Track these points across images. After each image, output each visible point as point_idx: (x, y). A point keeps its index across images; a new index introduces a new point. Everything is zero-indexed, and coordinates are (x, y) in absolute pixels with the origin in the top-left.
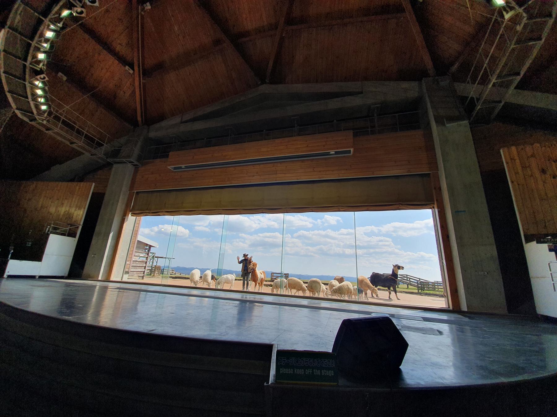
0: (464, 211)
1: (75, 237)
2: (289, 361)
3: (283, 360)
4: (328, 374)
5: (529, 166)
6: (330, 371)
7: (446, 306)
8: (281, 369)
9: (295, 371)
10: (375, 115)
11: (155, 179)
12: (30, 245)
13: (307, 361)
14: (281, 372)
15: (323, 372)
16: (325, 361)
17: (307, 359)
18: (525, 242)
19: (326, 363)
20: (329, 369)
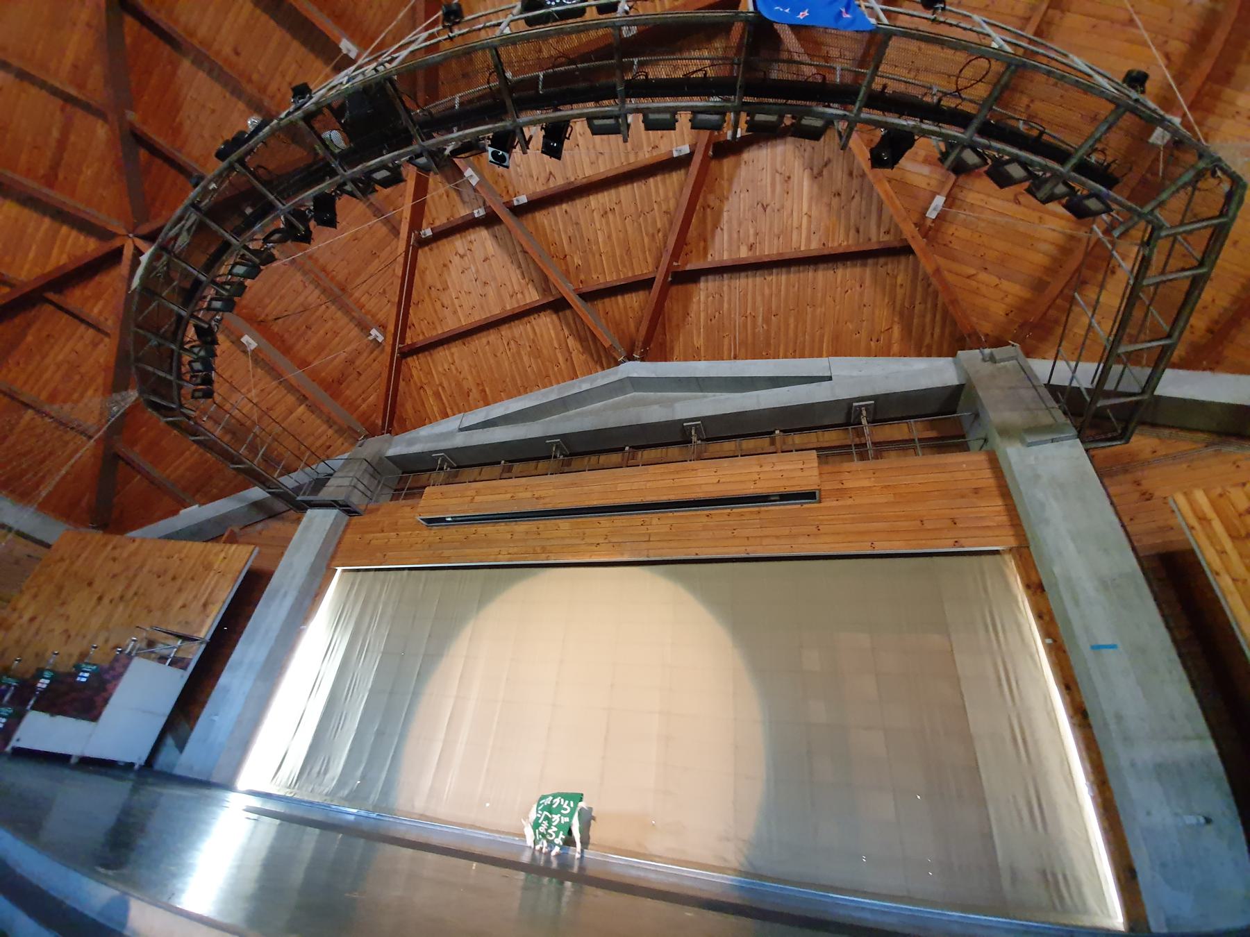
0: (1113, 647)
1: (185, 668)
7: (1094, 361)
11: (386, 543)
12: (84, 680)
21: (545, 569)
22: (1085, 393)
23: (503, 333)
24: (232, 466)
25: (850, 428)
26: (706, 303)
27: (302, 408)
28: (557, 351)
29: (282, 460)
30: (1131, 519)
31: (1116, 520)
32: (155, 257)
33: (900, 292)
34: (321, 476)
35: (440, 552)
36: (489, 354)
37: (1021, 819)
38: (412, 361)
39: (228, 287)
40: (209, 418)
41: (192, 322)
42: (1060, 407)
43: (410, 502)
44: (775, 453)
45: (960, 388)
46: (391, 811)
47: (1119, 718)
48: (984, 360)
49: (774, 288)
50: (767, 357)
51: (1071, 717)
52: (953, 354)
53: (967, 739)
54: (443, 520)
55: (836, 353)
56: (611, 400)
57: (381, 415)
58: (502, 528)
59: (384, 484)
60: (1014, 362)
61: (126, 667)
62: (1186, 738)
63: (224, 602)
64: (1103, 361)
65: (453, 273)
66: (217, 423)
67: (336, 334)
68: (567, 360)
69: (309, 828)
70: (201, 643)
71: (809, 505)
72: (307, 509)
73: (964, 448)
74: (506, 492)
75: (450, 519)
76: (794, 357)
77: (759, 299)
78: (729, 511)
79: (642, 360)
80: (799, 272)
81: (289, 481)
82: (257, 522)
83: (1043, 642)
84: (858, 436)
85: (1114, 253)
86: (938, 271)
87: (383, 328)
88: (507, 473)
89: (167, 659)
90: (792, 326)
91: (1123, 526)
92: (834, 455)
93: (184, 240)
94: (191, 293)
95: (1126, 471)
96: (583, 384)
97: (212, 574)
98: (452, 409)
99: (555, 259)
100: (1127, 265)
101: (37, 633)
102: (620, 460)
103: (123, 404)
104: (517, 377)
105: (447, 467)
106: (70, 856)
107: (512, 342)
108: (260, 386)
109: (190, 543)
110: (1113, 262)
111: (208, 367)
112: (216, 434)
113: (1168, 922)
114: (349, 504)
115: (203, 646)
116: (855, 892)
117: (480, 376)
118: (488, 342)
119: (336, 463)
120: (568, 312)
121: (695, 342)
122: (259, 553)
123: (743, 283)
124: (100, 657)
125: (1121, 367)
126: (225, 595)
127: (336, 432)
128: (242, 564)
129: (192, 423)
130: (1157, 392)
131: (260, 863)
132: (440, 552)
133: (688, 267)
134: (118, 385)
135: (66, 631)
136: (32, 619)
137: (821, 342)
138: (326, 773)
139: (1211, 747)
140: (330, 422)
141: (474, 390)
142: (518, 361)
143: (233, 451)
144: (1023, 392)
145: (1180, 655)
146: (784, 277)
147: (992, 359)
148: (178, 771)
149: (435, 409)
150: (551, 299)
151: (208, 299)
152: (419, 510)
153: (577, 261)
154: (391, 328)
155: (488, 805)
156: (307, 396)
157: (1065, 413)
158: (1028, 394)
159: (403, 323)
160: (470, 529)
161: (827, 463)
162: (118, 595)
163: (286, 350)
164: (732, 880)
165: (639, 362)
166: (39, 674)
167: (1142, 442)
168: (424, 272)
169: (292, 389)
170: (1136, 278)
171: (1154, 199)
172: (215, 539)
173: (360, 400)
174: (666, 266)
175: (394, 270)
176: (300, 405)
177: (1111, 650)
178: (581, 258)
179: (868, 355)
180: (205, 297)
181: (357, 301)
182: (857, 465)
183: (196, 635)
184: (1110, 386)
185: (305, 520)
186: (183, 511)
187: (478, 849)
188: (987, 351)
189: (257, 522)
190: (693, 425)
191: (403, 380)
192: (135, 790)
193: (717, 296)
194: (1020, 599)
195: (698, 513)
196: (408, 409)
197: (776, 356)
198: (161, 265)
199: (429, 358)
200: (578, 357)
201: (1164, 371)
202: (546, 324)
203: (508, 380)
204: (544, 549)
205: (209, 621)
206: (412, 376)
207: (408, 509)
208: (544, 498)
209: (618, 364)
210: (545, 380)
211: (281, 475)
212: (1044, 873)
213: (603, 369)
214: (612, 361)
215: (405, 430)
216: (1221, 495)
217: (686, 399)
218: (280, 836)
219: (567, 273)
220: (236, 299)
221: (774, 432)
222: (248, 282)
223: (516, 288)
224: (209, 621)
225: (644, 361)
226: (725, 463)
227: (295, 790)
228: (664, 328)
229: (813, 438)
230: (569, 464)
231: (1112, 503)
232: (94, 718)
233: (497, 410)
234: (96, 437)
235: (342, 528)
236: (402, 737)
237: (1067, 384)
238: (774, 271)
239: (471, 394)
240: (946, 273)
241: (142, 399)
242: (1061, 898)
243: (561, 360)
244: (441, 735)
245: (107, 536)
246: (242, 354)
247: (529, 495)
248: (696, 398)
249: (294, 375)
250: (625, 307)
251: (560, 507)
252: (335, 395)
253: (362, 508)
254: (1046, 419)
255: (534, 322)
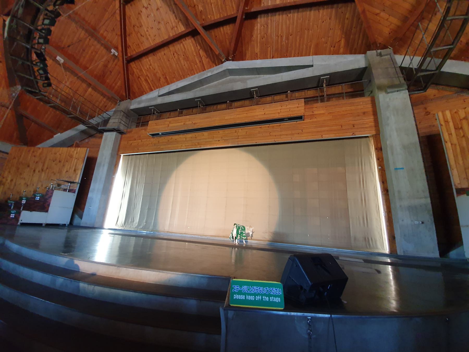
0: (402, 168)
1: (74, 192)
2: (242, 289)
3: (237, 288)
4: (275, 301)
5: (461, 128)
6: (278, 298)
7: (419, 56)
8: (235, 295)
9: (247, 297)
10: (324, 85)
11: (138, 144)
13: (257, 289)
14: (234, 298)
15: (271, 299)
16: (273, 289)
17: (257, 288)
18: (457, 195)
19: (274, 291)
20: (276, 296)
21: (196, 151)
22: (414, 69)
23: (171, 49)
24: (68, 116)
25: (318, 88)
26: (260, 30)
27: (90, 90)
28: (196, 57)
29: (88, 113)
30: (420, 123)
31: (414, 123)
32: (11, 21)
33: (346, 21)
34: (106, 119)
35: (159, 146)
36: (166, 60)
37: (360, 223)
38: (133, 65)
39: (44, 31)
40: (53, 96)
41: (33, 51)
42: (403, 77)
43: (143, 128)
44: (288, 101)
45: (365, 69)
46: (158, 231)
47: (399, 192)
48: (377, 55)
49: (291, 21)
50: (286, 56)
51: (382, 192)
52: (365, 53)
53: (346, 200)
54: (158, 134)
55: (316, 54)
56: (221, 80)
57: (124, 91)
58: (182, 136)
59: (132, 121)
60: (389, 56)
61: (52, 193)
62: (421, 198)
63: (82, 169)
64: (424, 56)
65: (143, 17)
66: (57, 98)
67: (96, 52)
68: (200, 61)
69: (131, 237)
70: (78, 184)
71: (299, 122)
72: (104, 133)
73: (362, 95)
74: (182, 122)
75: (161, 134)
76: (298, 56)
77: (284, 26)
78: (269, 125)
79: (233, 60)
80: (303, 11)
81: (93, 121)
82: (85, 139)
83: (378, 168)
84: (321, 92)
85: (438, 4)
86: (364, 11)
87: (116, 48)
88: (181, 114)
89: (67, 190)
90: (298, 40)
91: (416, 125)
92: (311, 101)
93: (21, 11)
94: (29, 37)
95: (422, 103)
96: (208, 73)
97: (73, 160)
98: (153, 87)
99: (190, 7)
100: (442, 10)
101: (15, 185)
102: (226, 106)
103: (16, 92)
104: (180, 71)
105: (156, 113)
106: (52, 251)
107: (175, 54)
108: (70, 80)
109: (62, 148)
110: (436, 9)
111: (46, 72)
112: (58, 102)
113: (404, 252)
114: (120, 129)
115: (79, 185)
116: (304, 245)
117: (163, 71)
118: (165, 54)
119: (111, 113)
120: (199, 37)
121: (256, 51)
122: (89, 150)
123: (278, 18)
124: (41, 190)
125: (430, 59)
126: (81, 167)
127: (107, 99)
128: (84, 154)
129: (47, 98)
130: (442, 70)
131: (118, 247)
132: (159, 146)
133: (253, 10)
134: (11, 83)
135: (25, 184)
136: (12, 180)
137: (310, 47)
138: (133, 221)
139: (429, 200)
140: (103, 95)
141: (162, 78)
142: (179, 63)
143: (67, 110)
144: (390, 69)
145: (426, 171)
146: (296, 14)
147: (380, 55)
148: (82, 225)
149: (147, 87)
150: (190, 30)
151: (37, 38)
152: (148, 130)
153: (201, 8)
154: (120, 48)
155: (189, 227)
156: (91, 83)
157: (405, 80)
158: (391, 71)
159: (125, 47)
160: (170, 137)
161: (308, 104)
162: (40, 169)
163: (77, 62)
164: (267, 243)
165: (231, 61)
166: (21, 199)
167: (431, 92)
168: (130, 18)
169: (83, 80)
170: (444, 18)
171: (55, 303)
172: (71, 146)
173: (114, 85)
174: (242, 9)
175: (116, 18)
176: (89, 88)
177: (401, 170)
178: (202, 7)
179: (329, 54)
180: (35, 38)
181: (102, 35)
182: (319, 104)
183: (75, 181)
184: (424, 67)
185: (104, 137)
186: (55, 136)
187: (187, 239)
188: (379, 51)
189: (85, 139)
190: (255, 90)
191: (131, 74)
192: (68, 232)
193: (266, 26)
194: (372, 154)
195: (257, 127)
196: (135, 87)
197: (290, 56)
198: (14, 24)
199: (140, 63)
200: (205, 60)
201: (447, 60)
202: (189, 43)
203: (176, 72)
204: (198, 143)
205: (78, 176)
206: (134, 72)
207: (144, 131)
208: (196, 123)
209: (222, 63)
210: (192, 72)
211: (89, 119)
212: (365, 239)
213: (216, 65)
214: (220, 61)
215: (136, 97)
216: (456, 112)
217: (251, 78)
218: (122, 239)
219: (196, 15)
220: (49, 37)
221: (288, 92)
222: (52, 28)
223: (174, 24)
224: (78, 176)
225: (234, 61)
226: (267, 105)
227: (124, 227)
228: (242, 44)
229: (303, 94)
230: (205, 110)
231: (414, 116)
232: (47, 211)
233: (173, 87)
234: (10, 107)
235: (119, 139)
236: (157, 210)
237: (407, 66)
238: (292, 11)
239: (161, 79)
240: (367, 13)
241: (23, 90)
242: (369, 245)
243: (198, 62)
244: (170, 208)
245: (30, 148)
246: (59, 66)
247: (190, 122)
248: (256, 78)
249: (82, 73)
250: (224, 33)
251: (204, 127)
252: (103, 82)
253: (125, 131)
254: (397, 82)
255: (184, 43)
